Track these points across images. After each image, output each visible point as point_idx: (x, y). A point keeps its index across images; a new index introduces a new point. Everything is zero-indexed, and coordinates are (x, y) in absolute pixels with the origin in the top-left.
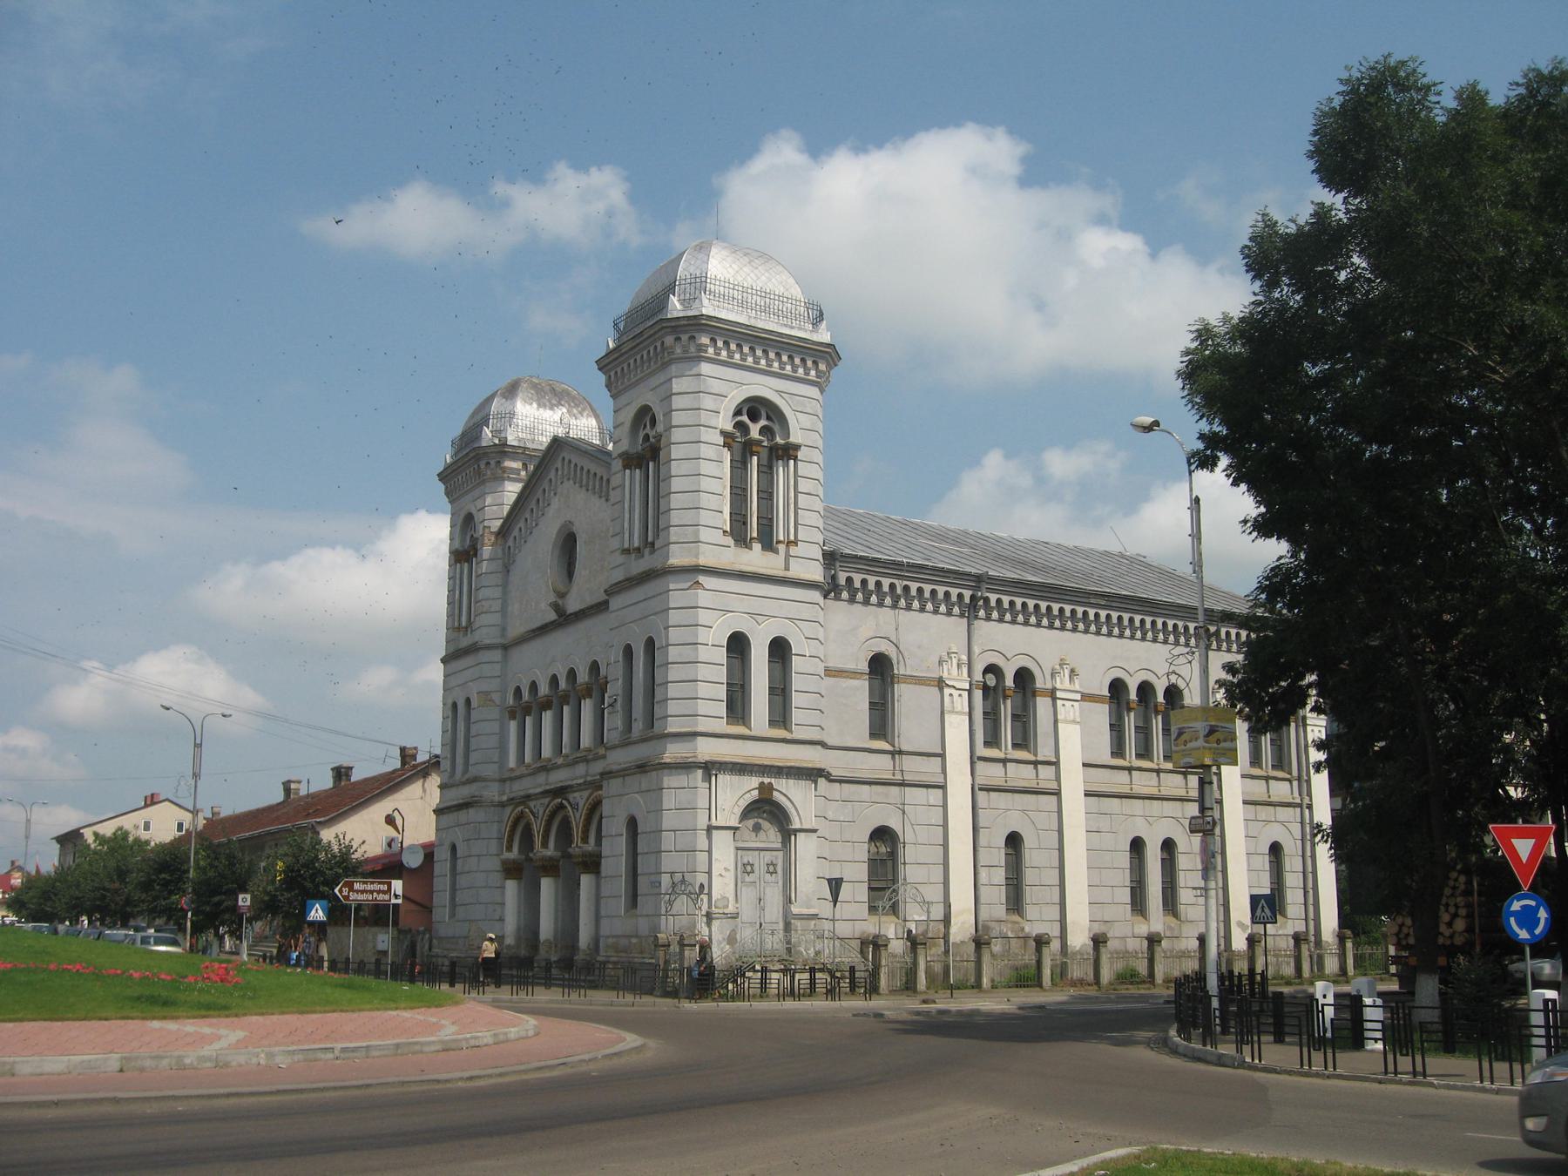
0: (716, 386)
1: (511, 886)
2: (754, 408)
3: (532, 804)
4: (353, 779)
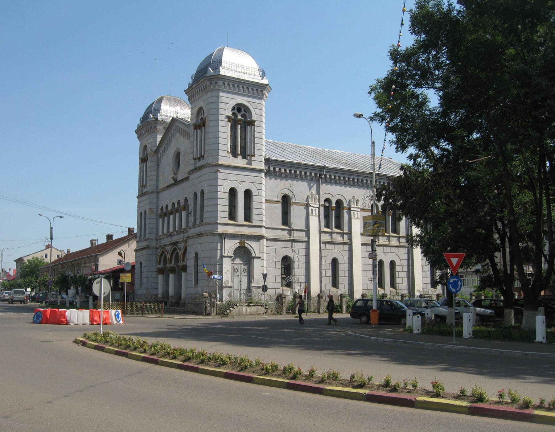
0: (225, 100)
1: (160, 277)
2: (239, 108)
3: (166, 248)
4: (114, 239)
